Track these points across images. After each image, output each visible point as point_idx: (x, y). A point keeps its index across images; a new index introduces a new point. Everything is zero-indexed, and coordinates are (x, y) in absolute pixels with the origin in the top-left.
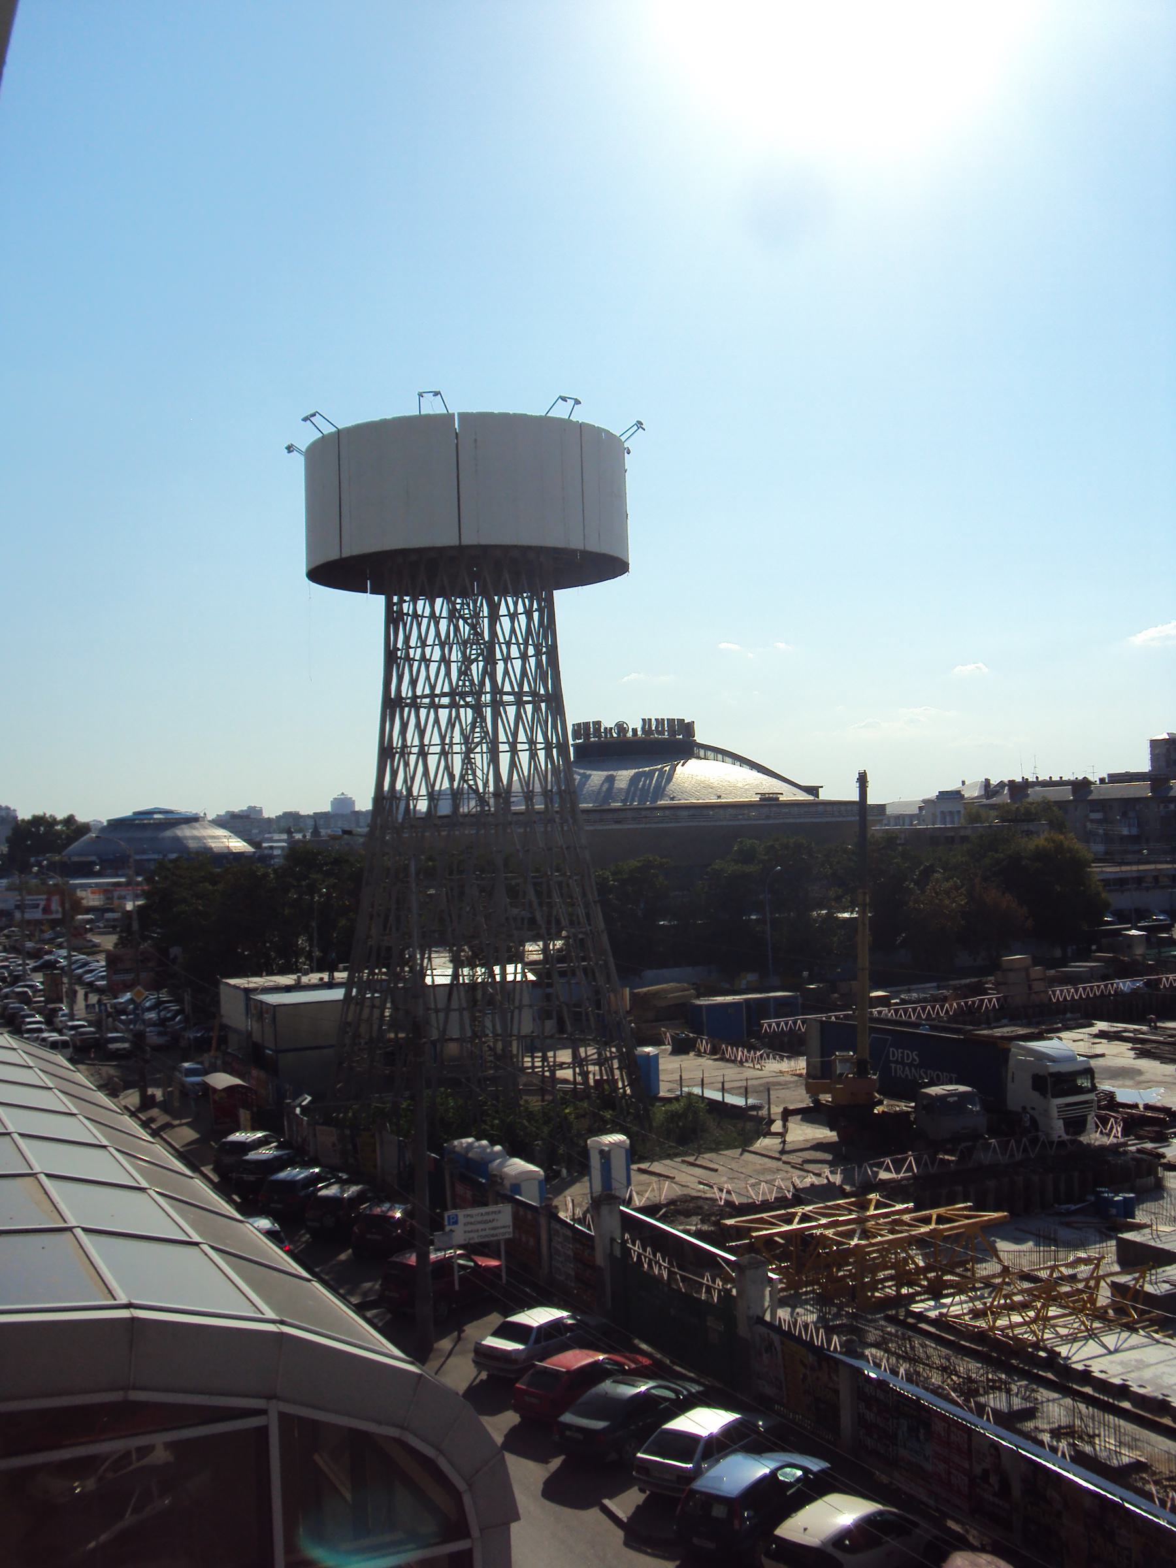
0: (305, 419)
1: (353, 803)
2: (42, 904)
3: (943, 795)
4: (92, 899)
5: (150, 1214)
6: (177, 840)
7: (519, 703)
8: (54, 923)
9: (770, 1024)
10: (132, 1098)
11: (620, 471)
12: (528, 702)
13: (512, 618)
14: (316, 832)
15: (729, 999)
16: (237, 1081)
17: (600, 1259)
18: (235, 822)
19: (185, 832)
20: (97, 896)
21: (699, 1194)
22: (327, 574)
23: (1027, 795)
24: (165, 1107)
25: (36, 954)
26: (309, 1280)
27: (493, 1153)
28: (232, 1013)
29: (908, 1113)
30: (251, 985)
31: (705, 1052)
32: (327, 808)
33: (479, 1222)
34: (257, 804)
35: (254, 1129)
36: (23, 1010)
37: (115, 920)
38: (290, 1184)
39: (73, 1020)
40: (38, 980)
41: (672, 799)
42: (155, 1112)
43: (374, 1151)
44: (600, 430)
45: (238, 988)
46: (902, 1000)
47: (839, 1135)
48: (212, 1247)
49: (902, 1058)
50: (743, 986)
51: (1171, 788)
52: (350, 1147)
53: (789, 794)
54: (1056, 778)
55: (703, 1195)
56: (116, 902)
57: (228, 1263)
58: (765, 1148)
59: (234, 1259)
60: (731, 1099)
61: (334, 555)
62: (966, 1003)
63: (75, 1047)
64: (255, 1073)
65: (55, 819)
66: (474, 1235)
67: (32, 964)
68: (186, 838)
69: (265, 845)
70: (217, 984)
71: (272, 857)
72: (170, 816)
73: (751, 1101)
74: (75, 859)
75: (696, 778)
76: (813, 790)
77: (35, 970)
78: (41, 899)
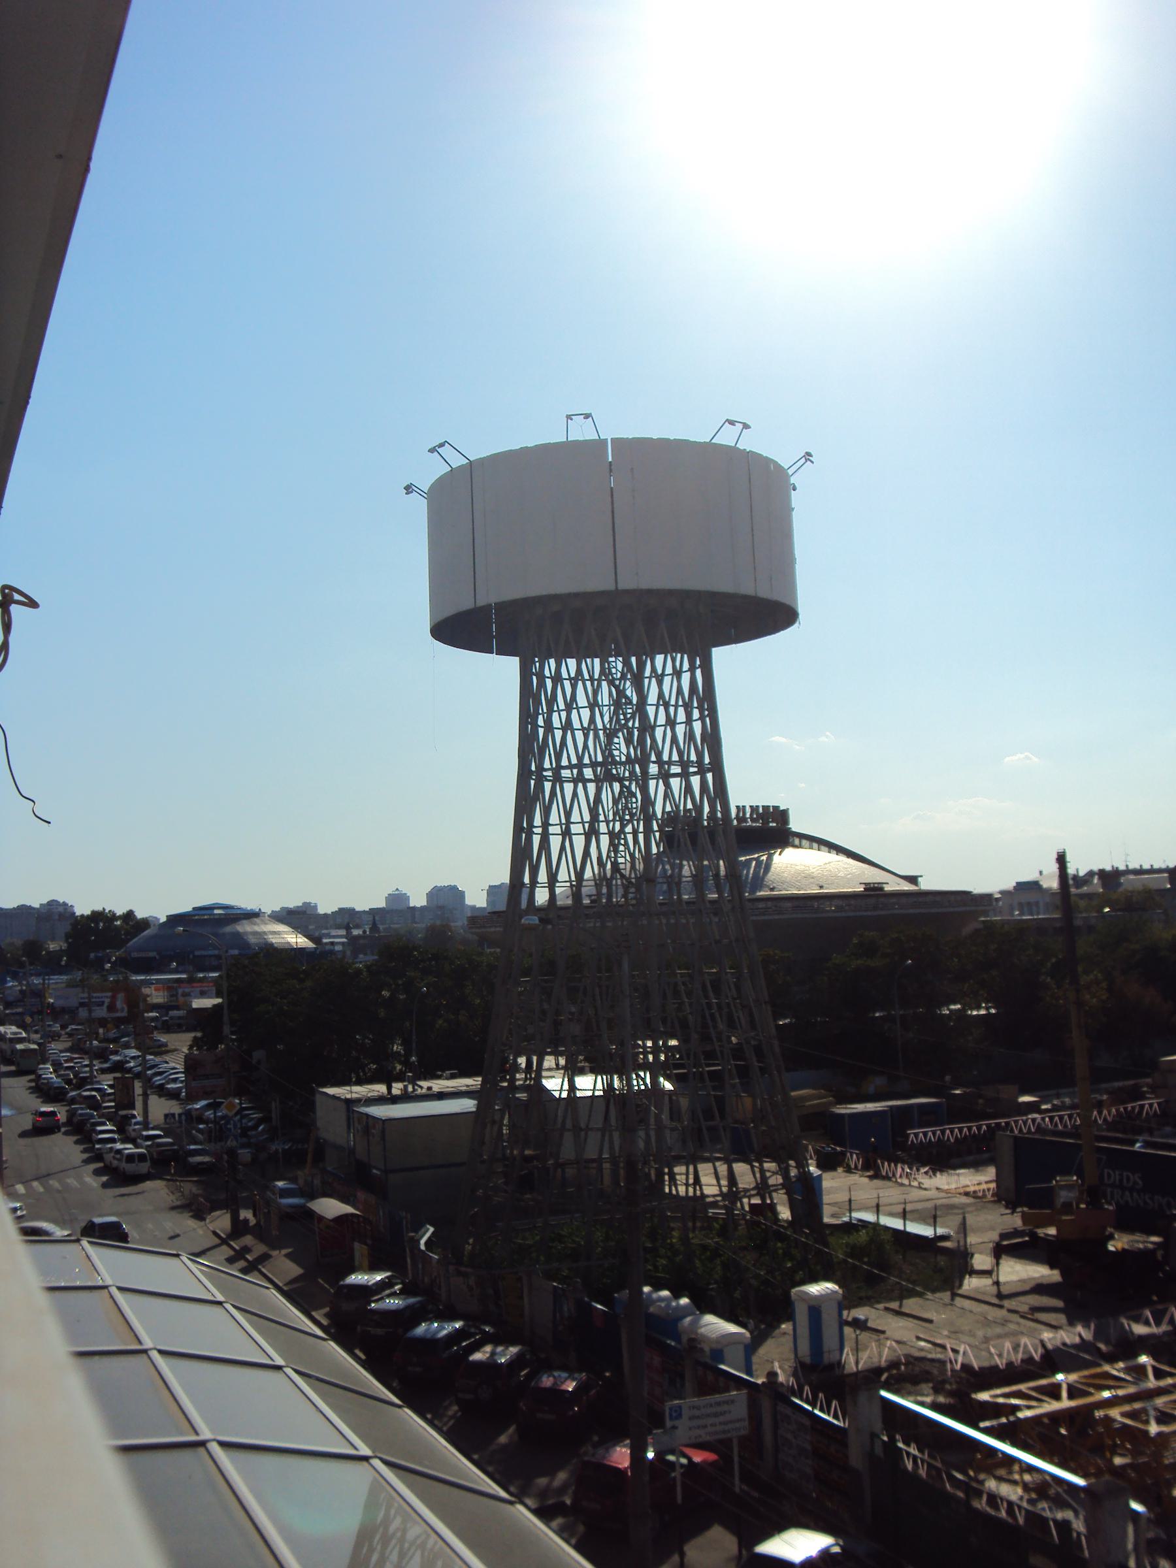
0: (432, 450)
2: (107, 1001)
3: (1020, 886)
4: (157, 997)
5: (228, 1332)
6: (238, 936)
7: (685, 775)
8: (118, 1022)
9: (917, 1135)
10: (221, 1221)
11: (788, 510)
12: (695, 773)
13: (668, 674)
14: (374, 928)
15: (870, 1107)
16: (348, 1209)
17: (856, 1457)
18: (297, 917)
19: (245, 927)
20: (161, 993)
21: (922, 1354)
22: (459, 629)
23: (1120, 884)
24: (260, 1232)
25: (102, 1055)
26: (324, 1339)
27: (678, 1307)
28: (330, 1127)
29: (1152, 1252)
30: (355, 1096)
31: (856, 1167)
32: (382, 904)
33: (708, 1415)
35: (373, 1268)
36: (92, 1116)
37: (179, 1018)
38: (430, 1343)
39: (147, 1129)
40: (106, 1082)
41: (772, 889)
42: (248, 1240)
44: (767, 461)
45: (338, 1098)
46: (1053, 1105)
47: (1062, 1275)
48: (386, 1463)
49: (1121, 1180)
50: (871, 1089)
53: (894, 885)
54: (1146, 866)
55: (929, 1356)
56: (181, 999)
57: (410, 1486)
58: (977, 1290)
59: (327, 1386)
60: (915, 1228)
61: (467, 604)
62: (1125, 1109)
63: (152, 1159)
64: (361, 1195)
65: (114, 914)
66: (698, 1432)
67: (97, 1065)
68: (246, 933)
69: (325, 941)
70: (313, 1092)
71: (332, 952)
72: (230, 911)
73: (940, 1231)
74: (135, 955)
75: (793, 868)
76: (913, 880)
77: (103, 1071)
78: (106, 997)
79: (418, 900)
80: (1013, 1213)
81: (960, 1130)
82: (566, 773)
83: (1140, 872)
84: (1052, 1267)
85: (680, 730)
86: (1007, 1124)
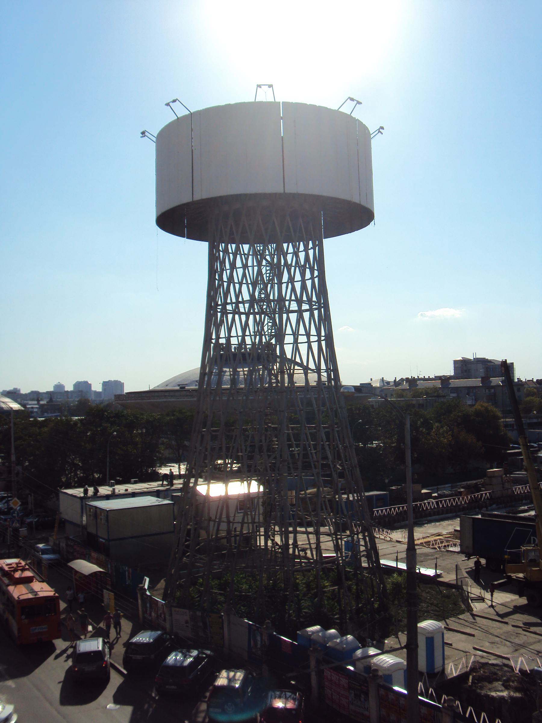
0: (168, 104)
1: (64, 387)
14: (51, 400)
28: (68, 511)
32: (52, 389)
34: (18, 387)
43: (222, 628)
45: (75, 496)
51: (450, 383)
52: (201, 624)
54: (427, 377)
62: (474, 496)
69: (28, 406)
70: (57, 494)
79: (69, 387)
80: (468, 560)
81: (399, 508)
82: (229, 307)
83: (424, 379)
84: (521, 596)
85: (298, 286)
86: (421, 504)
